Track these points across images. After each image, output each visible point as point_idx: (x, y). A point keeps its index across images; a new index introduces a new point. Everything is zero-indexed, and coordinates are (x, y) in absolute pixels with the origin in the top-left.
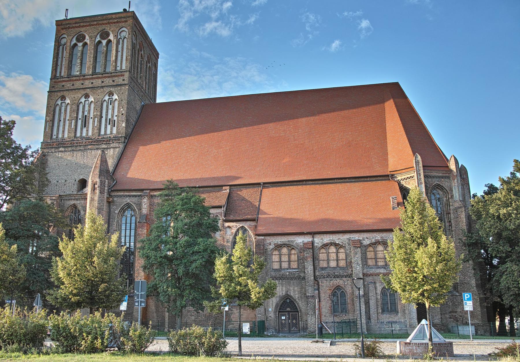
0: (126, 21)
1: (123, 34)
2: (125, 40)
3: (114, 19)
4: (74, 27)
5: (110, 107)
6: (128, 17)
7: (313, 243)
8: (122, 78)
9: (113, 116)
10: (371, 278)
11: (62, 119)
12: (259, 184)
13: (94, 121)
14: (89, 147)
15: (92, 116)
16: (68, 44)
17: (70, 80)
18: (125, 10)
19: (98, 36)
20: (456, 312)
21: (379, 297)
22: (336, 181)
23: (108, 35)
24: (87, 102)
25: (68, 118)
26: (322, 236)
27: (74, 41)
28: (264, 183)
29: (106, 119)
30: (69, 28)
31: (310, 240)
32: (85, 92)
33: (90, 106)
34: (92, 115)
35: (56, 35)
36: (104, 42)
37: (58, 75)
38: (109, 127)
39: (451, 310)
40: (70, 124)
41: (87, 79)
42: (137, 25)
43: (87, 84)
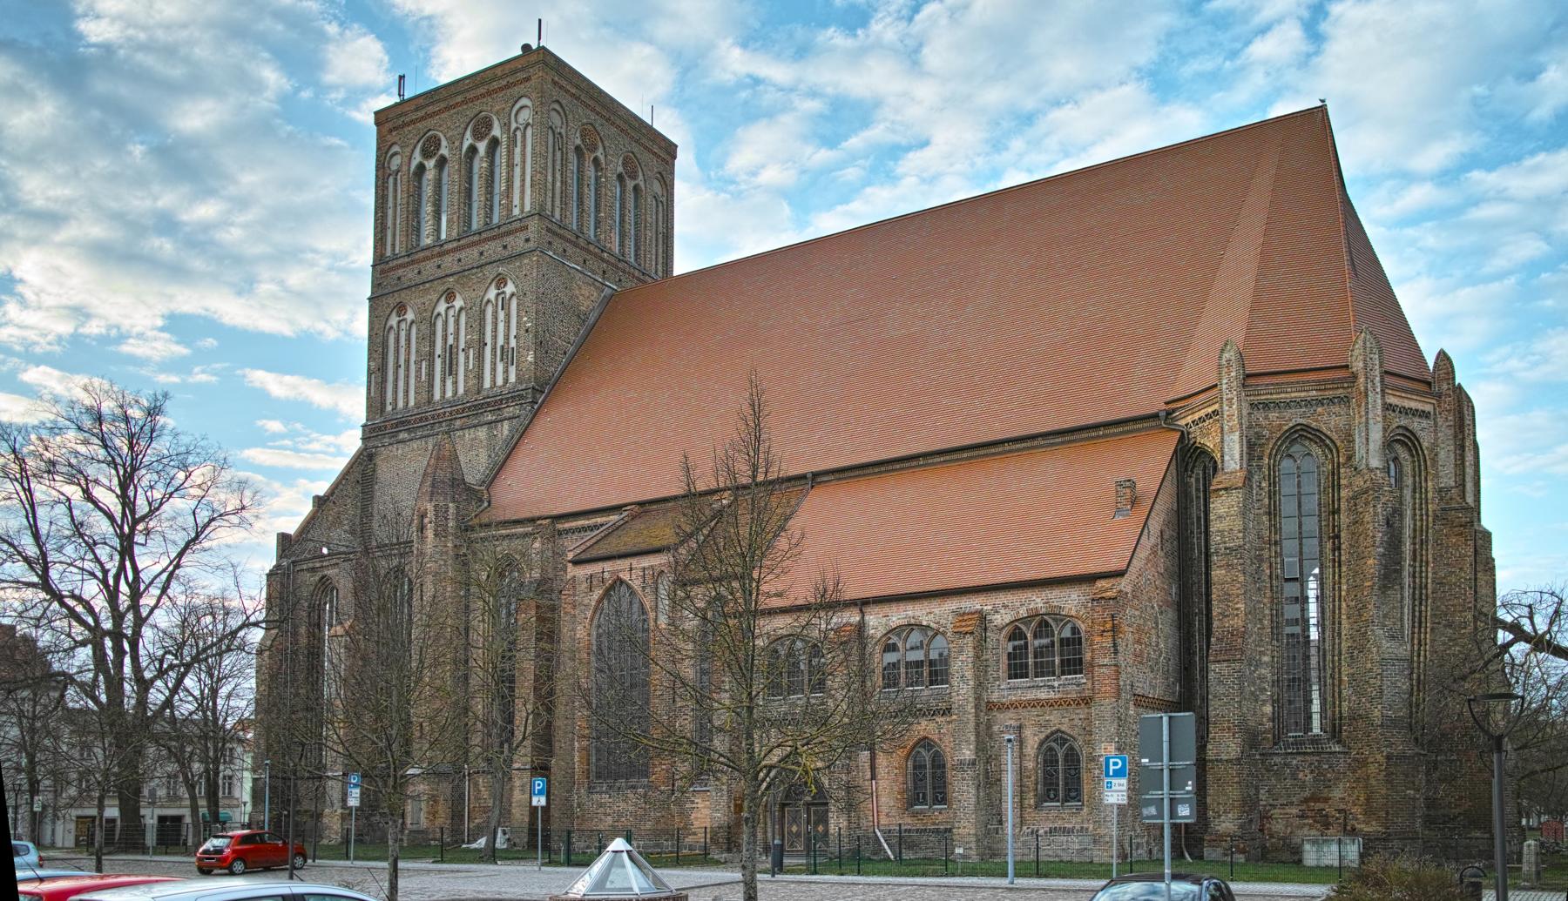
0: (528, 79)
1: (525, 116)
2: (529, 131)
3: (501, 78)
4: (413, 122)
5: (501, 315)
6: (538, 71)
7: (861, 627)
8: (522, 236)
9: (507, 338)
10: (1011, 714)
11: (402, 362)
12: (803, 477)
13: (467, 358)
14: (458, 423)
15: (462, 345)
16: (405, 168)
17: (413, 262)
18: (526, 48)
19: (468, 133)
20: (1326, 800)
21: (1030, 765)
22: (1007, 447)
23: (489, 126)
24: (451, 312)
25: (413, 358)
26: (886, 609)
27: (417, 158)
28: (815, 475)
29: (494, 349)
30: (405, 125)
31: (856, 618)
32: (443, 288)
33: (457, 322)
34: (462, 345)
35: (379, 149)
36: (482, 147)
37: (389, 253)
38: (500, 367)
39: (1307, 794)
40: (419, 370)
41: (448, 252)
42: (564, 83)
43: (449, 262)
